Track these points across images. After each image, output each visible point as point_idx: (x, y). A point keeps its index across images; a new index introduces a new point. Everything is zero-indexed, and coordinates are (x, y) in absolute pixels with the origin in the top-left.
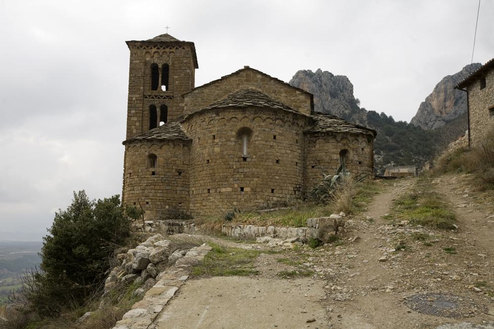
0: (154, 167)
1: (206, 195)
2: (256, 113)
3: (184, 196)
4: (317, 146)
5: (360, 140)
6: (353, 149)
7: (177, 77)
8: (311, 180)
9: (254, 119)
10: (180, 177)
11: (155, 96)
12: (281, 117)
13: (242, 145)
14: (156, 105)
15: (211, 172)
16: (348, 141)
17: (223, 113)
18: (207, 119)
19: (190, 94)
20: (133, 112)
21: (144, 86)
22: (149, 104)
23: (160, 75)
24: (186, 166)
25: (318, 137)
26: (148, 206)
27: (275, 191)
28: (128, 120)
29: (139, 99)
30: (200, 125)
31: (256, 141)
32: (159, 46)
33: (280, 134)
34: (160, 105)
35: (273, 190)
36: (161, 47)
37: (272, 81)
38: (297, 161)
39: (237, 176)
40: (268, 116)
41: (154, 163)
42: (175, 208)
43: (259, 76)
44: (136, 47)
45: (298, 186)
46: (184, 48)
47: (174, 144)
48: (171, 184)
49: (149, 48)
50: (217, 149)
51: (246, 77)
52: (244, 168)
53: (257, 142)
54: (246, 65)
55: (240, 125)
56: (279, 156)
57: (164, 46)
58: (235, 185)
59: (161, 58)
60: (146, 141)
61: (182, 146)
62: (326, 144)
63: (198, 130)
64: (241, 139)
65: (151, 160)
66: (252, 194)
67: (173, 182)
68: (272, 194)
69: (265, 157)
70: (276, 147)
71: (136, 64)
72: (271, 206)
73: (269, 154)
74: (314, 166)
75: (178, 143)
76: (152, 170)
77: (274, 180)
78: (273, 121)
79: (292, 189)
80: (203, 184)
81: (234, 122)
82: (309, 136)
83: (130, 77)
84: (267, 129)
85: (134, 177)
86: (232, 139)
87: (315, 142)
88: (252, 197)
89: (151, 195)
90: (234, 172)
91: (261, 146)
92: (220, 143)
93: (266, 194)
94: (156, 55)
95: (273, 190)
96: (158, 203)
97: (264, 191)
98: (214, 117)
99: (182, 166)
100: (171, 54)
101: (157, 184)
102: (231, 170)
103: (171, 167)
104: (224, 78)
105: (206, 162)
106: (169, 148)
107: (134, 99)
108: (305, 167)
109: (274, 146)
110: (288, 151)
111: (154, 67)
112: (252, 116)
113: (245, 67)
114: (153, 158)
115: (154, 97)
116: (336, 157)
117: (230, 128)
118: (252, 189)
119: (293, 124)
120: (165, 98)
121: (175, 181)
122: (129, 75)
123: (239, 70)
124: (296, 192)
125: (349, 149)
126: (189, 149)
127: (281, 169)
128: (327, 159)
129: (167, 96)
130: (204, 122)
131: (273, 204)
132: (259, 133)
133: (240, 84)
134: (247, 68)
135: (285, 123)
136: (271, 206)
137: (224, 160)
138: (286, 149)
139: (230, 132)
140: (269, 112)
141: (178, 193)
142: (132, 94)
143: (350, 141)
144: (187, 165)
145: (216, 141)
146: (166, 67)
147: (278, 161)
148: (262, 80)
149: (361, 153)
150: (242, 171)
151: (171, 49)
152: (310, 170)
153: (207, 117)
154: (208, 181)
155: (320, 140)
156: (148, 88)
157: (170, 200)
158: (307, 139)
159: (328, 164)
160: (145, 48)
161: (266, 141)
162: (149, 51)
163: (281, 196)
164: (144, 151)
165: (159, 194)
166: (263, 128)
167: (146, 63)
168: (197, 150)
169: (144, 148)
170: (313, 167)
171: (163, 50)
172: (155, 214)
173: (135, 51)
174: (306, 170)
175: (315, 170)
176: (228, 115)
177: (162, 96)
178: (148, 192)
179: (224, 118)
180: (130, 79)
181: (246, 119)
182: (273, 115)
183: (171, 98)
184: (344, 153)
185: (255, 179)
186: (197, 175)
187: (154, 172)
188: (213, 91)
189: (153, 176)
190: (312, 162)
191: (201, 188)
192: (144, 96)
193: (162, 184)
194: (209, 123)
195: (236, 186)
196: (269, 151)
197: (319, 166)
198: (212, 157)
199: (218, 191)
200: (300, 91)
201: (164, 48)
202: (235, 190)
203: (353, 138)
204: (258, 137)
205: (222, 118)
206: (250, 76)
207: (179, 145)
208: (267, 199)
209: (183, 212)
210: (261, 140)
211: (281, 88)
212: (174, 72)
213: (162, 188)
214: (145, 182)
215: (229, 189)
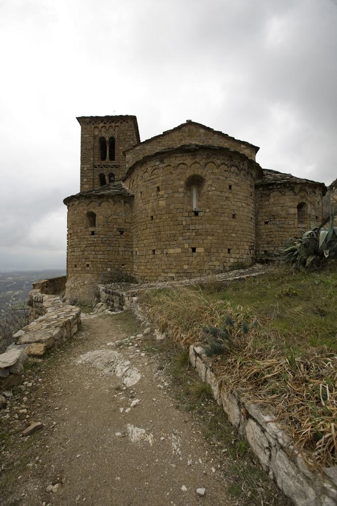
0: (95, 227)
1: (151, 256)
2: (208, 157)
3: (127, 257)
4: (272, 200)
5: (317, 193)
6: (311, 203)
7: (122, 148)
8: (264, 237)
9: (206, 165)
10: (122, 236)
11: (104, 166)
13: (191, 197)
15: (156, 230)
16: (306, 194)
17: (169, 159)
19: (131, 151)
20: (85, 180)
21: (93, 158)
22: (99, 173)
23: (108, 148)
25: (273, 189)
26: (88, 268)
28: (81, 187)
30: (142, 177)
31: (209, 191)
32: (105, 121)
33: (236, 184)
34: (108, 173)
35: (229, 250)
37: (216, 135)
39: (188, 234)
40: (222, 162)
41: (95, 222)
42: (118, 270)
43: (202, 131)
45: (252, 244)
46: (127, 122)
47: (114, 201)
48: (112, 245)
49: (97, 123)
50: (162, 203)
51: (189, 132)
52: (196, 224)
53: (210, 193)
54: (189, 119)
55: (189, 173)
57: (110, 121)
58: (185, 245)
59: (108, 132)
60: (84, 198)
61: (123, 203)
62: (282, 197)
63: (140, 183)
64: (190, 190)
65: (91, 219)
66: (206, 256)
68: (228, 255)
69: (220, 210)
71: (86, 138)
72: (228, 268)
73: (224, 207)
74: (268, 222)
75: (118, 200)
76: (91, 229)
78: (228, 167)
79: (247, 247)
80: (146, 245)
81: (183, 169)
82: (261, 189)
83: (82, 149)
84: (221, 178)
85: (74, 238)
86: (181, 190)
87: (269, 195)
88: (206, 259)
89: (91, 256)
90: (184, 229)
91: (215, 198)
92: (165, 196)
93: (222, 255)
94: (103, 130)
95: (229, 250)
98: (158, 165)
99: (124, 224)
100: (117, 127)
101: (97, 245)
102: (180, 228)
103: (111, 225)
104: (166, 133)
105: (149, 218)
106: (109, 205)
107: (85, 169)
108: (257, 224)
110: (243, 204)
111: (102, 141)
113: (187, 121)
114: (92, 216)
116: (294, 211)
117: (178, 177)
118: (206, 250)
119: (248, 173)
120: (112, 167)
122: (80, 148)
123: (181, 125)
125: (307, 202)
126: (131, 206)
128: (283, 214)
130: (146, 173)
131: (230, 267)
132: (213, 182)
134: (190, 123)
135: (241, 171)
136: (228, 268)
137: (171, 215)
138: (242, 201)
139: (178, 181)
140: (223, 157)
141: (121, 254)
143: (307, 193)
144: (130, 223)
145: (161, 193)
146: (112, 140)
147: (234, 216)
148: (205, 134)
149: (317, 207)
150: (194, 228)
151: (116, 123)
152: (262, 227)
153: (149, 167)
154: (153, 241)
155: (275, 193)
156: (97, 159)
157: (111, 262)
158: (259, 192)
159: (284, 219)
160: (93, 124)
161: (221, 192)
164: (83, 208)
165: (99, 256)
166: (218, 176)
167: (95, 137)
168: (140, 205)
169: (82, 206)
170: (266, 223)
171: (109, 125)
172: (96, 278)
173: (85, 126)
175: (269, 226)
176: (175, 161)
177: (109, 166)
178: (88, 254)
179: (170, 165)
181: (196, 164)
182: (228, 160)
183: (117, 167)
184: (301, 206)
185: (210, 238)
186: (140, 234)
188: (155, 147)
191: (144, 249)
192: (94, 166)
193: (102, 245)
194: (152, 173)
195: (186, 246)
197: (274, 222)
198: (157, 213)
200: (246, 145)
201: (110, 123)
202: (185, 251)
203: (311, 190)
205: (167, 166)
206: (193, 131)
207: (119, 201)
208: (223, 260)
210: (215, 190)
211: (225, 142)
212: (119, 144)
213: (103, 248)
214: (85, 243)
215: (179, 250)
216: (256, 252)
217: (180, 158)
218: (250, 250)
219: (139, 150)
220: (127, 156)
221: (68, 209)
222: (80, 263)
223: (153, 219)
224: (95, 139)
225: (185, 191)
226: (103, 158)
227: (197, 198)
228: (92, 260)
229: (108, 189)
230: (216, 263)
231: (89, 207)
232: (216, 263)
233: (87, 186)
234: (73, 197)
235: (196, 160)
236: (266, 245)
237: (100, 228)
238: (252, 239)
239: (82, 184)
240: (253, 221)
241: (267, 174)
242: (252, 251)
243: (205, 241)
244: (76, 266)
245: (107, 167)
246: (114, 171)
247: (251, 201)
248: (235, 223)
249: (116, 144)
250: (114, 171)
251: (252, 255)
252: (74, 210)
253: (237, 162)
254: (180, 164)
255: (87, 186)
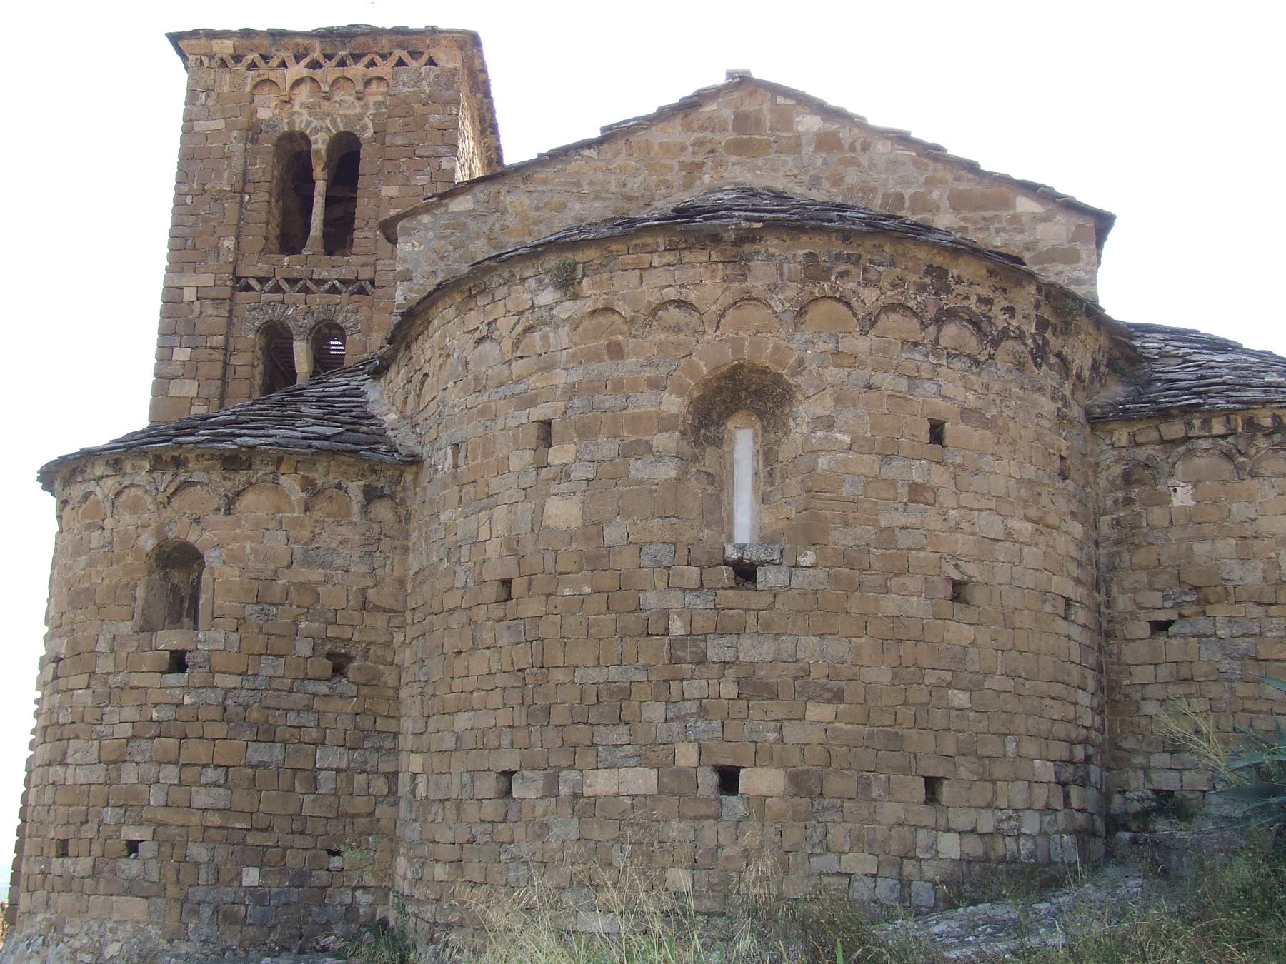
3: (361, 805)
9: (802, 313)
10: (343, 686)
11: (287, 280)
12: (973, 303)
14: (291, 324)
15: (522, 659)
18: (504, 324)
19: (426, 219)
20: (182, 354)
22: (260, 319)
24: (380, 620)
25: (1187, 438)
26: (131, 867)
27: (946, 791)
29: (214, 294)
33: (967, 414)
34: (309, 322)
35: (932, 784)
36: (329, 57)
38: (1071, 590)
39: (694, 688)
42: (300, 879)
44: (217, 61)
45: (1079, 753)
46: (431, 62)
49: (275, 62)
54: (738, 66)
56: (971, 558)
59: (326, 106)
64: (718, 442)
66: (796, 816)
67: (293, 719)
68: (926, 815)
70: (947, 499)
73: (904, 540)
74: (1170, 623)
75: (332, 480)
76: (170, 639)
77: (938, 719)
78: (924, 327)
79: (1045, 771)
80: (469, 740)
81: (677, 329)
84: (886, 381)
88: (794, 835)
89: (156, 796)
92: (581, 472)
93: (890, 811)
95: (932, 784)
96: (198, 852)
97: (875, 793)
100: (374, 87)
101: (193, 729)
102: (653, 651)
105: (492, 591)
107: (190, 294)
109: (934, 490)
110: (1016, 524)
112: (792, 291)
115: (285, 286)
117: (648, 373)
118: (799, 782)
119: (1039, 354)
120: (334, 290)
121: (308, 708)
124: (1074, 791)
126: (404, 519)
127: (983, 639)
129: (343, 282)
130: (487, 345)
133: (700, 166)
135: (995, 343)
142: (181, 271)
145: (560, 454)
147: (959, 591)
150: (729, 656)
151: (372, 64)
154: (503, 718)
159: (1257, 611)
160: (253, 65)
161: (886, 458)
162: (273, 75)
163: (986, 823)
166: (863, 374)
167: (254, 132)
172: (172, 922)
173: (208, 78)
174: (1113, 646)
175: (1172, 647)
177: (319, 282)
179: (608, 310)
180: (179, 203)
181: (748, 310)
182: (922, 288)
183: (362, 291)
185: (818, 712)
187: (183, 653)
189: (173, 679)
190: (1155, 598)
191: (457, 765)
192: (238, 279)
193: (219, 730)
194: (516, 346)
195: (687, 756)
196: (900, 519)
197: (1203, 625)
199: (564, 790)
201: (342, 64)
204: (830, 423)
208: (895, 847)
209: (351, 909)
215: (642, 780)
216: (1106, 797)
217: (664, 277)
218: (1064, 785)
219: (470, 214)
220: (404, 246)
221: (60, 517)
222: (89, 831)
223: (509, 598)
224: (254, 141)
225: (688, 449)
226: (291, 241)
227: (755, 489)
228: (160, 815)
229: (281, 423)
230: (858, 863)
231: (168, 513)
232: (858, 863)
233: (189, 389)
234: (88, 455)
235: (749, 284)
236: (1165, 759)
237: (220, 635)
238: (1075, 722)
239: (163, 380)
240: (1081, 615)
241: (1163, 355)
242: (1074, 791)
243: (793, 733)
244: (63, 849)
245: (306, 290)
246: (346, 310)
247: (1062, 505)
248: (968, 632)
249: (366, 166)
250: (346, 310)
251: (1080, 818)
252: (89, 527)
253: (973, 299)
254: (664, 305)
255: (189, 389)
